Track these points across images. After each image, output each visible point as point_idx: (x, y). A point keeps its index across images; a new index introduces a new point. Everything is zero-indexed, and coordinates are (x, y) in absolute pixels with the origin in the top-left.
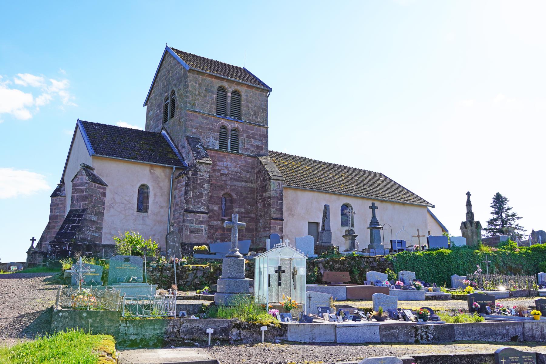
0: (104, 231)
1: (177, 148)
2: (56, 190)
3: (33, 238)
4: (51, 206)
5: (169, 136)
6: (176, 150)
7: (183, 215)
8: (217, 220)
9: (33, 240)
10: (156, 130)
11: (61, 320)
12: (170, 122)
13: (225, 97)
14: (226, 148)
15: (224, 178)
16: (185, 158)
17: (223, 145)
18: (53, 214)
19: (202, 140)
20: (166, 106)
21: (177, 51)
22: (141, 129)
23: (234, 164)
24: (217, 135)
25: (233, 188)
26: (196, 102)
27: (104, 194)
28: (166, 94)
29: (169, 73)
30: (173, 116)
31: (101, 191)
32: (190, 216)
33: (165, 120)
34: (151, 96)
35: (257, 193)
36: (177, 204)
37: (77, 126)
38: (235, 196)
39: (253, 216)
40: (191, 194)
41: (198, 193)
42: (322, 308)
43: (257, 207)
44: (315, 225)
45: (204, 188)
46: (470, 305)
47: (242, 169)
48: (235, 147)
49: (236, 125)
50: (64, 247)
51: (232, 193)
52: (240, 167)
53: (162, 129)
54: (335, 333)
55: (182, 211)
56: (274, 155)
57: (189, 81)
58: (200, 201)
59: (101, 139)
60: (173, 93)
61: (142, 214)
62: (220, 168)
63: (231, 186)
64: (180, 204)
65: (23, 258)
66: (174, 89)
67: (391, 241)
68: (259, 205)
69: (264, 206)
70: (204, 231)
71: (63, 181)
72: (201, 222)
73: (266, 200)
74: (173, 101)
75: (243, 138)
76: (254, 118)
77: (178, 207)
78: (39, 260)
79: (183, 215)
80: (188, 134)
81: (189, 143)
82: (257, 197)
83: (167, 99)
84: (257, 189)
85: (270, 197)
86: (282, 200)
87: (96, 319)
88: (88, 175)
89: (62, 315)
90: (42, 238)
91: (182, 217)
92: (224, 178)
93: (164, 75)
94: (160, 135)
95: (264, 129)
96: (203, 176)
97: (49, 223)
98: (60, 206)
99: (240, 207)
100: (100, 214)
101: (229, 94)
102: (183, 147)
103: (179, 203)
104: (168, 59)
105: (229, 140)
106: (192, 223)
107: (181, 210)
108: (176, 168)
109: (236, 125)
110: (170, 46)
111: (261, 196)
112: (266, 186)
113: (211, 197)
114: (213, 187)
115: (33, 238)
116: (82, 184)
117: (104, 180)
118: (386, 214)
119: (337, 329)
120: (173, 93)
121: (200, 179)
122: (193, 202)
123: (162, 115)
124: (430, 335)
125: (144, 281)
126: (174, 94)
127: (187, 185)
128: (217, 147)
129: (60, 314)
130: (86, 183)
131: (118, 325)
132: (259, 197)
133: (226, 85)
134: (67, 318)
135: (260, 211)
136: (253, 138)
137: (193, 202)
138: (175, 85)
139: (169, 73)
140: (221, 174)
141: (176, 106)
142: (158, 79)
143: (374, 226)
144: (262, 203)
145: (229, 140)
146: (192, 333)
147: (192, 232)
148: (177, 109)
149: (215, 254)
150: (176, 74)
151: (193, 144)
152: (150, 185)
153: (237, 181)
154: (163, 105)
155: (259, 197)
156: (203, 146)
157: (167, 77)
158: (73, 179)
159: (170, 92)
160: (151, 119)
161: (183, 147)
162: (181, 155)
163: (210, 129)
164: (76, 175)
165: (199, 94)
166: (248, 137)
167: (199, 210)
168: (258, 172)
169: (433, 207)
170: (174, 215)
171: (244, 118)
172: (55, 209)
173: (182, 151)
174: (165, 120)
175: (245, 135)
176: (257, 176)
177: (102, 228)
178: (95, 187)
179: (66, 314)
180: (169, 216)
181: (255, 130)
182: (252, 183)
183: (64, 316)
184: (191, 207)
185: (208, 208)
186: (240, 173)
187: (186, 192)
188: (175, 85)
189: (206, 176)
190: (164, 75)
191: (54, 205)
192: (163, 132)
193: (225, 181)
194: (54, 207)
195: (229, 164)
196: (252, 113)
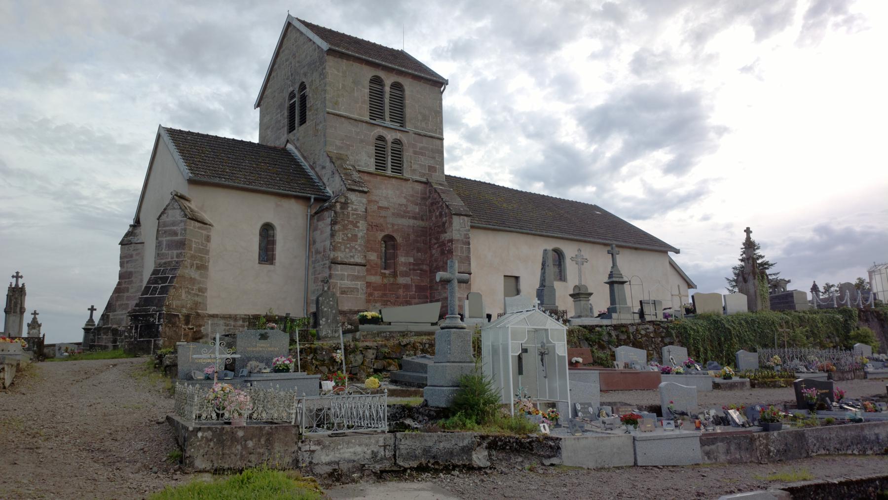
0: (209, 294)
1: (313, 168)
2: (128, 235)
3: (92, 307)
4: (121, 258)
5: (299, 151)
6: (312, 173)
7: (330, 268)
8: (376, 274)
9: (92, 309)
10: (280, 143)
11: (200, 445)
12: (300, 131)
13: (381, 93)
14: (384, 168)
15: (383, 213)
16: (327, 184)
17: (380, 164)
18: (125, 270)
19: (351, 157)
20: (292, 108)
21: (304, 23)
22: (247, 138)
23: (398, 192)
24: (372, 149)
25: (396, 227)
26: (340, 100)
27: (208, 238)
28: (291, 89)
29: (294, 56)
30: (303, 121)
31: (204, 232)
32: (339, 270)
33: (291, 128)
34: (266, 93)
35: (430, 235)
36: (317, 252)
37: (159, 136)
38: (399, 240)
39: (425, 267)
40: (339, 238)
41: (350, 235)
42: (581, 404)
43: (432, 256)
44: (513, 280)
45: (358, 227)
46: (799, 394)
47: (408, 200)
48: (398, 166)
49: (398, 135)
50: (152, 320)
51: (395, 235)
52: (405, 198)
53: (288, 141)
54: (635, 450)
55: (327, 262)
56: (452, 180)
57: (327, 67)
58: (353, 247)
59: (198, 156)
60: (303, 86)
61: (267, 267)
62: (377, 199)
63: (393, 225)
64: (324, 251)
65: (79, 337)
66: (304, 80)
67: (641, 302)
68: (434, 251)
69: (442, 253)
70: (361, 291)
71: (137, 223)
72: (356, 278)
73: (444, 245)
74: (303, 99)
75: (407, 155)
76: (424, 125)
77: (319, 256)
78: (105, 339)
79: (330, 268)
80: (330, 148)
81: (332, 162)
82: (430, 239)
83: (294, 96)
84: (430, 228)
85: (451, 241)
86: (469, 244)
87: (259, 441)
88: (183, 209)
89: (202, 437)
90: (110, 307)
91: (327, 270)
92: (383, 213)
93: (287, 60)
94: (285, 152)
95: (438, 142)
96: (356, 210)
97: (119, 284)
98: (135, 257)
99: (407, 255)
100: (202, 267)
101: (387, 89)
102: (324, 167)
103: (322, 250)
104: (292, 35)
105: (389, 158)
106: (341, 279)
107: (321, 262)
108: (315, 199)
109: (398, 135)
110: (293, 15)
111: (437, 239)
112: (444, 224)
113: (368, 241)
114: (372, 227)
115: (92, 307)
116: (174, 224)
117: (206, 217)
118: (630, 265)
119: (636, 443)
120: (303, 86)
121: (353, 214)
122: (343, 247)
123: (286, 121)
124: (772, 449)
125: (296, 371)
126: (305, 88)
127: (334, 223)
128: (372, 169)
129: (200, 434)
130: (181, 221)
131: (296, 448)
132: (434, 241)
133: (382, 74)
134: (211, 440)
135: (436, 260)
136: (422, 154)
137: (343, 247)
138: (305, 74)
139: (294, 56)
140: (380, 208)
141: (308, 106)
142: (276, 66)
143: (615, 282)
144: (439, 249)
145: (389, 158)
146: (416, 457)
147: (343, 293)
148: (310, 110)
149: (390, 324)
150: (306, 56)
151: (338, 163)
152: (276, 223)
153: (403, 217)
154: (287, 105)
155: (434, 241)
156: (354, 167)
157: (291, 63)
158: (160, 216)
159: (297, 86)
160: (268, 128)
161: (324, 167)
162: (320, 179)
163: (362, 141)
164: (165, 209)
165: (344, 86)
166: (415, 153)
167: (352, 260)
168: (432, 204)
169: (677, 251)
170: (314, 268)
171: (409, 127)
172: (127, 262)
173: (322, 173)
174: (291, 128)
175: (411, 150)
176: (430, 211)
177: (206, 289)
178: (194, 227)
179: (209, 434)
180: (307, 269)
181: (425, 143)
182: (423, 220)
183: (206, 438)
184: (340, 256)
185: (365, 256)
186: (406, 206)
187: (332, 235)
188: (305, 74)
189: (361, 210)
190: (287, 60)
191: (126, 257)
192: (290, 146)
193: (385, 217)
194: (126, 260)
195: (391, 195)
196: (420, 117)
